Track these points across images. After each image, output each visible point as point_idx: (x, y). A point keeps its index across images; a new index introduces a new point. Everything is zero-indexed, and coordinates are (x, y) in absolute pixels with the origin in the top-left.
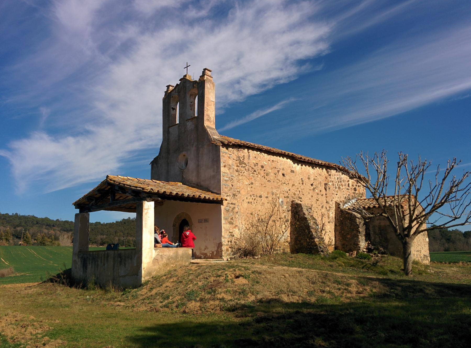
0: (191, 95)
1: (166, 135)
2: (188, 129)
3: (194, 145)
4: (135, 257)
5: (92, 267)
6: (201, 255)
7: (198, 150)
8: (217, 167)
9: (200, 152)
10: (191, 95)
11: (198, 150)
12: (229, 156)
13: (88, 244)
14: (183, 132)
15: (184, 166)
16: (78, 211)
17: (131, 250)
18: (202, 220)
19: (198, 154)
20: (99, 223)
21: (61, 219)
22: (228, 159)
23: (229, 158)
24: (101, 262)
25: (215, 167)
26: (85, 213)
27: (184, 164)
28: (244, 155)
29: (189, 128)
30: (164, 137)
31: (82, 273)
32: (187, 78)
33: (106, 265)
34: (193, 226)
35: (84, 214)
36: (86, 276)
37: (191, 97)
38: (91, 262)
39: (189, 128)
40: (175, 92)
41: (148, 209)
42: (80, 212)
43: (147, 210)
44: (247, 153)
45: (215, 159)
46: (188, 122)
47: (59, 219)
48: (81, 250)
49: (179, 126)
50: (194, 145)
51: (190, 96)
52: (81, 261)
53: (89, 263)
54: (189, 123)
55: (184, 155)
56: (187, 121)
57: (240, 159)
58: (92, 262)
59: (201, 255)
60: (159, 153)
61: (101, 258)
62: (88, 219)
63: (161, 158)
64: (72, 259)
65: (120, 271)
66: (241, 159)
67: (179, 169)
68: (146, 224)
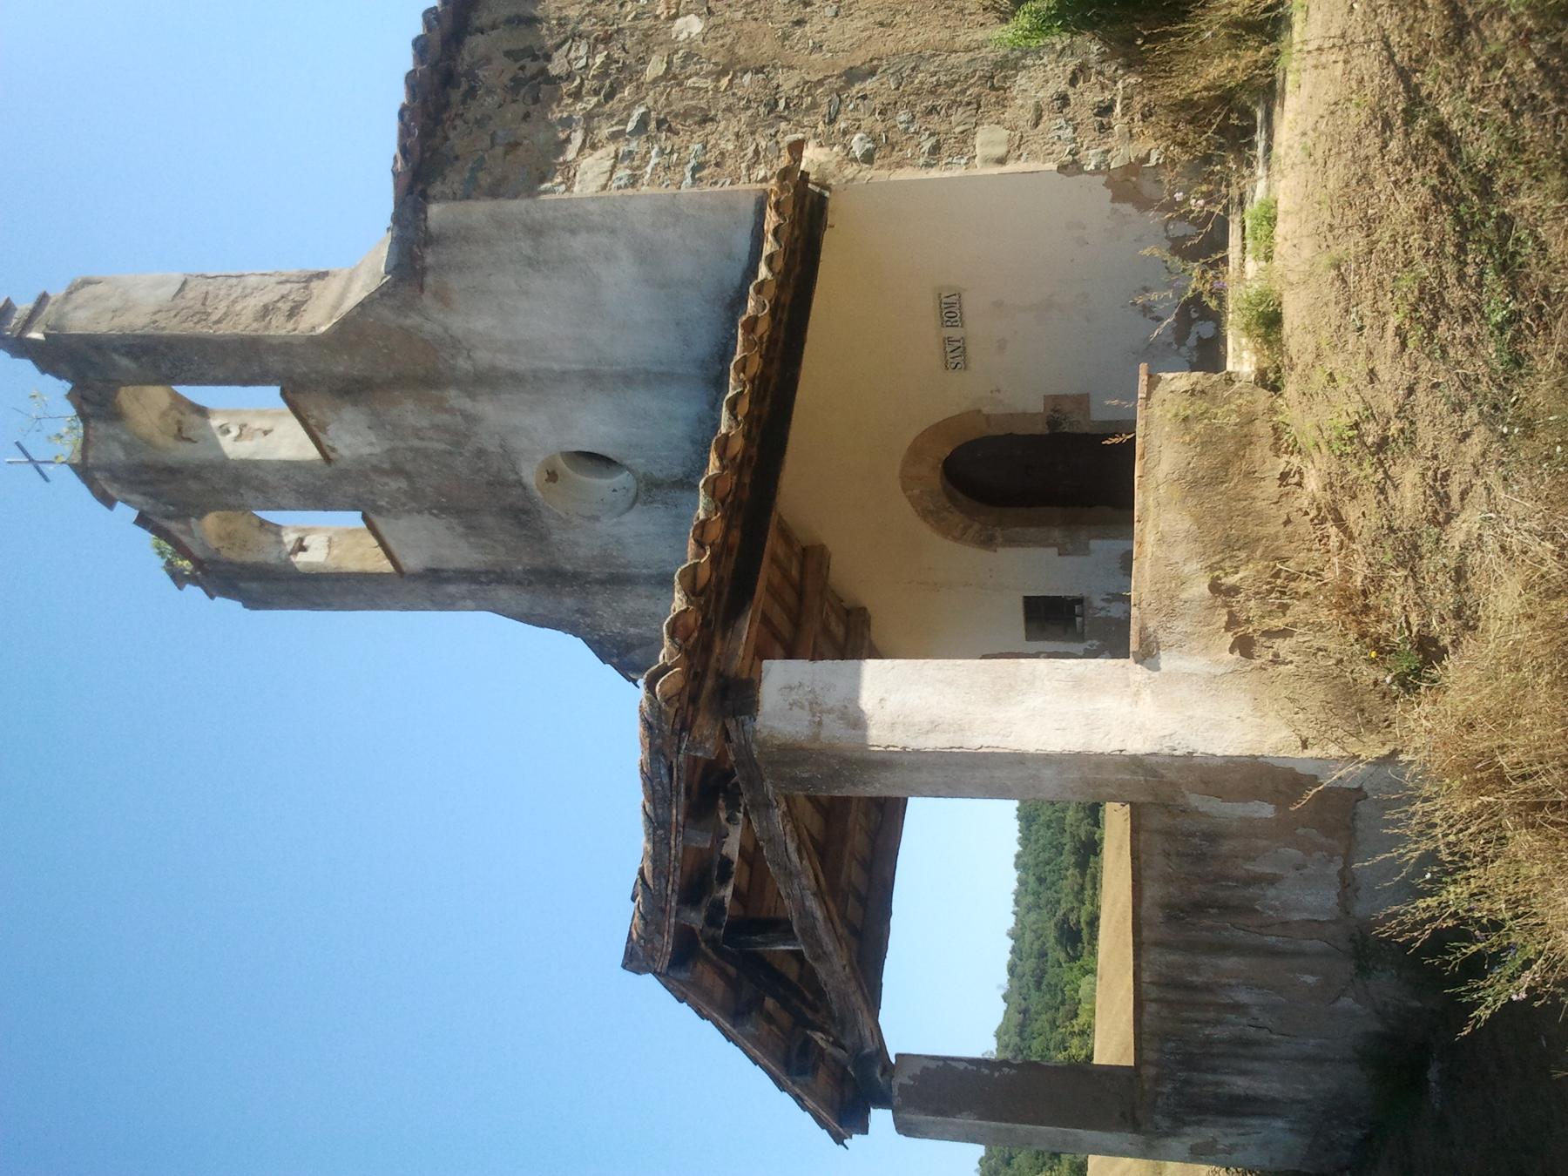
0: (180, 435)
1: (451, 589)
2: (377, 450)
3: (467, 404)
4: (1196, 811)
5: (1243, 1073)
6: (1192, 341)
7: (486, 381)
8: (573, 232)
9: (503, 361)
10: (180, 435)
11: (486, 381)
12: (499, 150)
13: (1084, 1070)
14: (404, 484)
15: (622, 479)
16: (880, 1119)
17: (1142, 837)
18: (949, 340)
19: (516, 379)
20: (1018, 856)
21: (999, 987)
22: (521, 151)
23: (514, 146)
24: (1217, 1023)
25: (579, 244)
26: (895, 1083)
27: (608, 481)
28: (508, 54)
29: (371, 444)
30: (469, 603)
31: (1279, 1124)
32: (77, 459)
33: (1243, 997)
34: (986, 410)
35: (901, 1086)
36: (1303, 1102)
37: (191, 434)
38: (1209, 1077)
39: (371, 444)
40: (190, 532)
41: (815, 706)
42: (884, 1102)
43: (826, 719)
44: (494, 33)
45: (528, 251)
46: (333, 450)
47: (1002, 992)
48: (1123, 1115)
49: (378, 510)
50: (467, 404)
51: (189, 439)
52: (1199, 1123)
53: (1218, 1084)
54: (338, 445)
55: (552, 476)
56: (332, 455)
57: (533, 78)
58: (1214, 1070)
59: (1192, 341)
60: (557, 627)
61: (1184, 1021)
62: (932, 1065)
63: (588, 620)
64: (1184, 1160)
65: (1296, 916)
66: (528, 73)
67: (638, 505)
68: (934, 726)
